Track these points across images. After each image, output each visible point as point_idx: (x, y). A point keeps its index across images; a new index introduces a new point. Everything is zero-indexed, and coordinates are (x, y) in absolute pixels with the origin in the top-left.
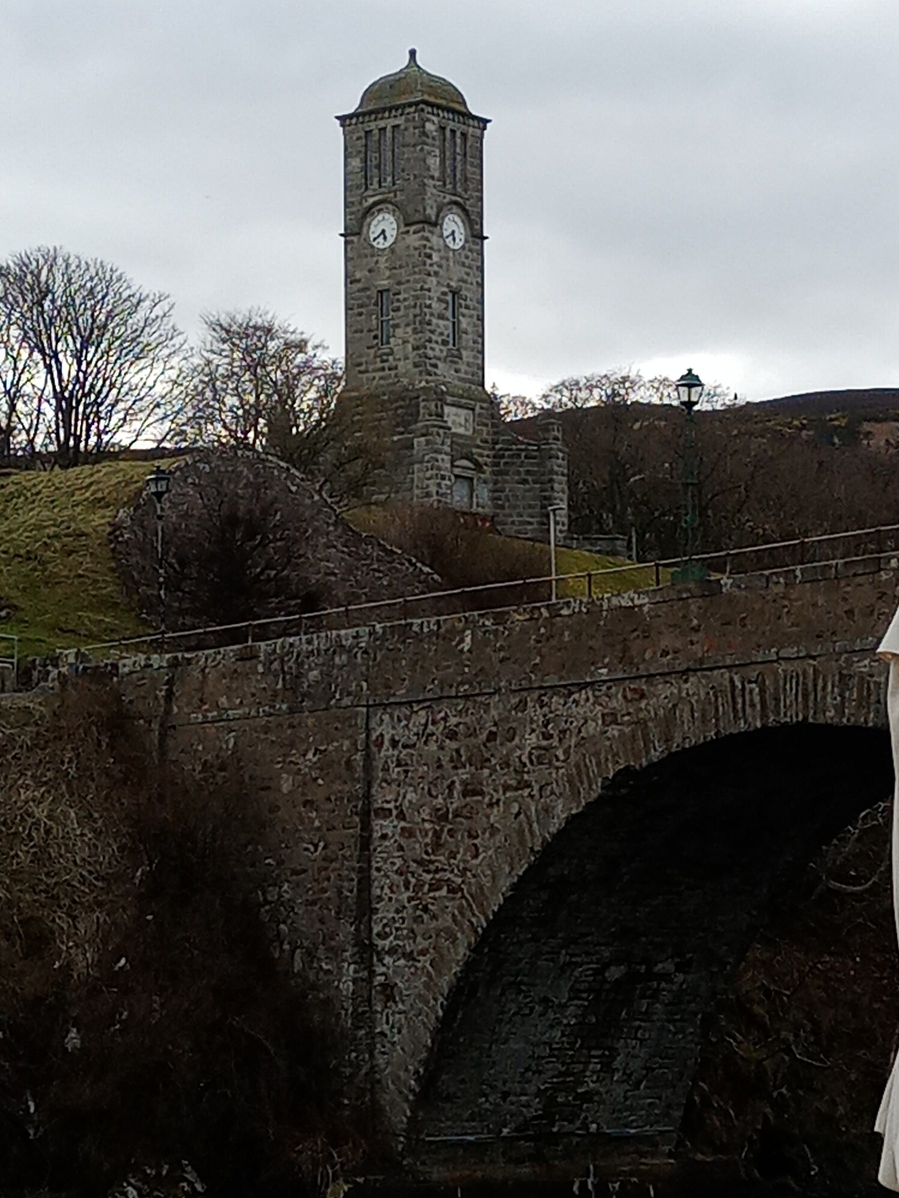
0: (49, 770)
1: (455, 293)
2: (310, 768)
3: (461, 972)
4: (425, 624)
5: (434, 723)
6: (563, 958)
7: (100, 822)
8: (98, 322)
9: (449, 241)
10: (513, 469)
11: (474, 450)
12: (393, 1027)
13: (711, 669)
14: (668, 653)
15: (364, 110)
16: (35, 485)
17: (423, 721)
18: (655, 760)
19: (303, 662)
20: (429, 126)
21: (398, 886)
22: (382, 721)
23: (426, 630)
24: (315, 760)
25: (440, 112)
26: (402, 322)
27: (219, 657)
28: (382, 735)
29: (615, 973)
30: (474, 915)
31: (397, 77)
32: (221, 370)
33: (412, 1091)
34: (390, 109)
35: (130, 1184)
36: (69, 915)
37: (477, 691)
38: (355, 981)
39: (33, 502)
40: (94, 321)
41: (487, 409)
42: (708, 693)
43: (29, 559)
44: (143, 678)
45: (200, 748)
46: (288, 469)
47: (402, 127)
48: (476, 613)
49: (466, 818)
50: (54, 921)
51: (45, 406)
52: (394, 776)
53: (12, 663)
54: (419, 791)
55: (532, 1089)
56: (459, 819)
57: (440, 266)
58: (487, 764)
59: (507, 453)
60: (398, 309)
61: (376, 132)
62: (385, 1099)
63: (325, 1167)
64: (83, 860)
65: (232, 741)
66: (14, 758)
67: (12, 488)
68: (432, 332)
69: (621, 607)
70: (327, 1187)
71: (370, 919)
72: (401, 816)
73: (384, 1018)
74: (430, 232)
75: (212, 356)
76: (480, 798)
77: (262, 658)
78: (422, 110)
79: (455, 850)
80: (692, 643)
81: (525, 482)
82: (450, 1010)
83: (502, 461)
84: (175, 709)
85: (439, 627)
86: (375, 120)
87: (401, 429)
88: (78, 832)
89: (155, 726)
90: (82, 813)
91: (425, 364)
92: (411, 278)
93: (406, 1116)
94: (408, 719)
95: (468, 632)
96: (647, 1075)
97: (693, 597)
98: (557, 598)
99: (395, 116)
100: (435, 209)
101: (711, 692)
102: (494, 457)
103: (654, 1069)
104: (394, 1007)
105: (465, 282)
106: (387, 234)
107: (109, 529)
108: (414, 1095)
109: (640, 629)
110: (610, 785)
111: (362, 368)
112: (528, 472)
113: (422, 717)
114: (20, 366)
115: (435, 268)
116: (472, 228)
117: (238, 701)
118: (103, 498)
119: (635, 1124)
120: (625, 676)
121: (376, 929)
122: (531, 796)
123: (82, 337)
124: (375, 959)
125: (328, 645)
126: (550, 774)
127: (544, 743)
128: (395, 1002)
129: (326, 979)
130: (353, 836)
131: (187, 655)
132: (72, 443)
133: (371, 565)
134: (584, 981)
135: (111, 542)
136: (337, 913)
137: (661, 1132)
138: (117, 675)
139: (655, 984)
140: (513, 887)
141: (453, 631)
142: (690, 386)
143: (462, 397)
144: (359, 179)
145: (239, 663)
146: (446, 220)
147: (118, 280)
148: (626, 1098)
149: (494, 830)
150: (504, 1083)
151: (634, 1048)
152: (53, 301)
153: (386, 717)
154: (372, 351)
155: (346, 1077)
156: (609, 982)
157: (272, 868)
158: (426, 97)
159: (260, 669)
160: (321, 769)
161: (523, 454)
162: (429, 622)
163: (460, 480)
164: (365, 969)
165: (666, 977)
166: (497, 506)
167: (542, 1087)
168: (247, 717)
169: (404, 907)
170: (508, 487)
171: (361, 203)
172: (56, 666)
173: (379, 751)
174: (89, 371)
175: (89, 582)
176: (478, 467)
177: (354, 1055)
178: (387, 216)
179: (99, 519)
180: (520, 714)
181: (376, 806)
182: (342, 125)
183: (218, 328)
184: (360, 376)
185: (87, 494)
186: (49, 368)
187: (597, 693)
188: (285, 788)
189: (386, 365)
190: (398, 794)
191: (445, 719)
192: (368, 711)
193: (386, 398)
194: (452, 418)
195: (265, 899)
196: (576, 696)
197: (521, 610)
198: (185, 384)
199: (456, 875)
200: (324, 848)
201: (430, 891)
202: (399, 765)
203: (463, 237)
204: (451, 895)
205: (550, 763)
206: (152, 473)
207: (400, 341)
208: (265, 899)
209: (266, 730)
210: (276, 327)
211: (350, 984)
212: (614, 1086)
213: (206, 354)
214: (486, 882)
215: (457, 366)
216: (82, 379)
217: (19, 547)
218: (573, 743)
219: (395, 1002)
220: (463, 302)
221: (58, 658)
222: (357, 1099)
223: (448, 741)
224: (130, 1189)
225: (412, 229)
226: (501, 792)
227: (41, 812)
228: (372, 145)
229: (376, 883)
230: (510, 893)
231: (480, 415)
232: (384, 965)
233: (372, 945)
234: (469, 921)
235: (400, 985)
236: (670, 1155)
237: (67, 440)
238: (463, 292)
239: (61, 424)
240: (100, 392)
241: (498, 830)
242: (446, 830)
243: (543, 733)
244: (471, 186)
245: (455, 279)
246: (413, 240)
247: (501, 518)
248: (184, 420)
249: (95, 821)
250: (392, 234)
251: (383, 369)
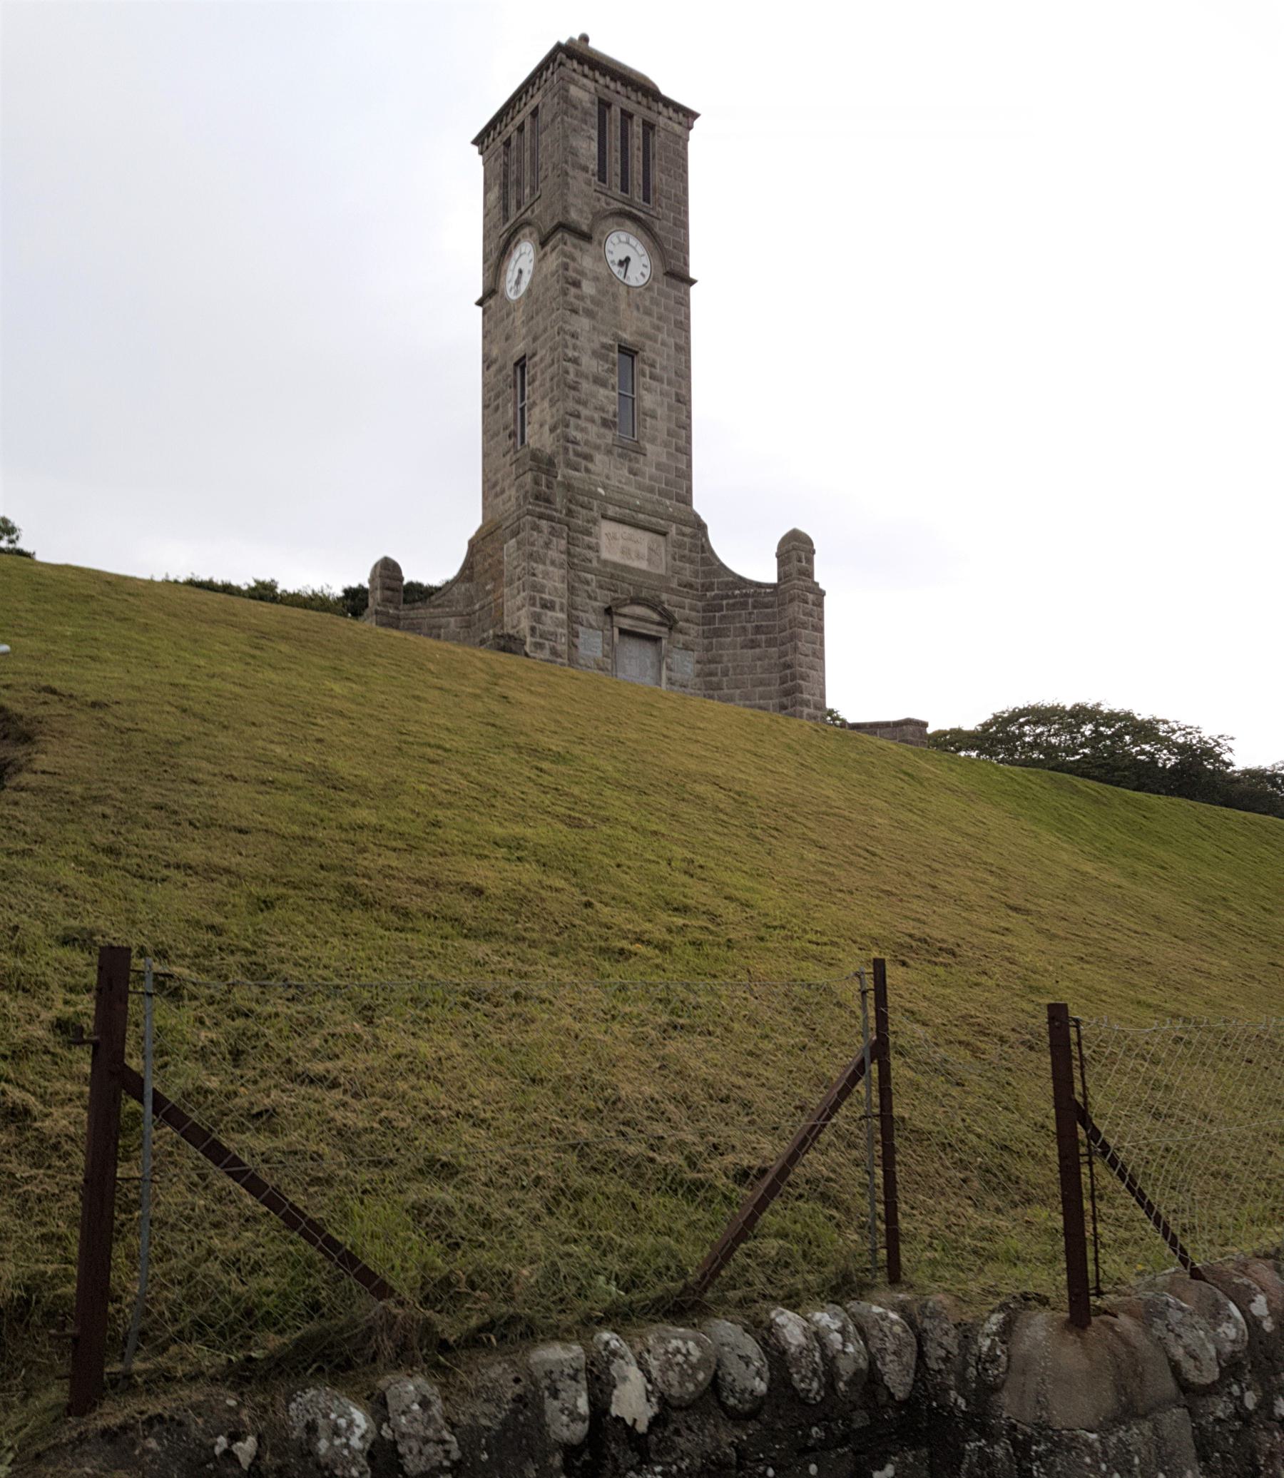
74: (575, 246)
81: (753, 644)
170: (726, 654)
238: (647, 354)
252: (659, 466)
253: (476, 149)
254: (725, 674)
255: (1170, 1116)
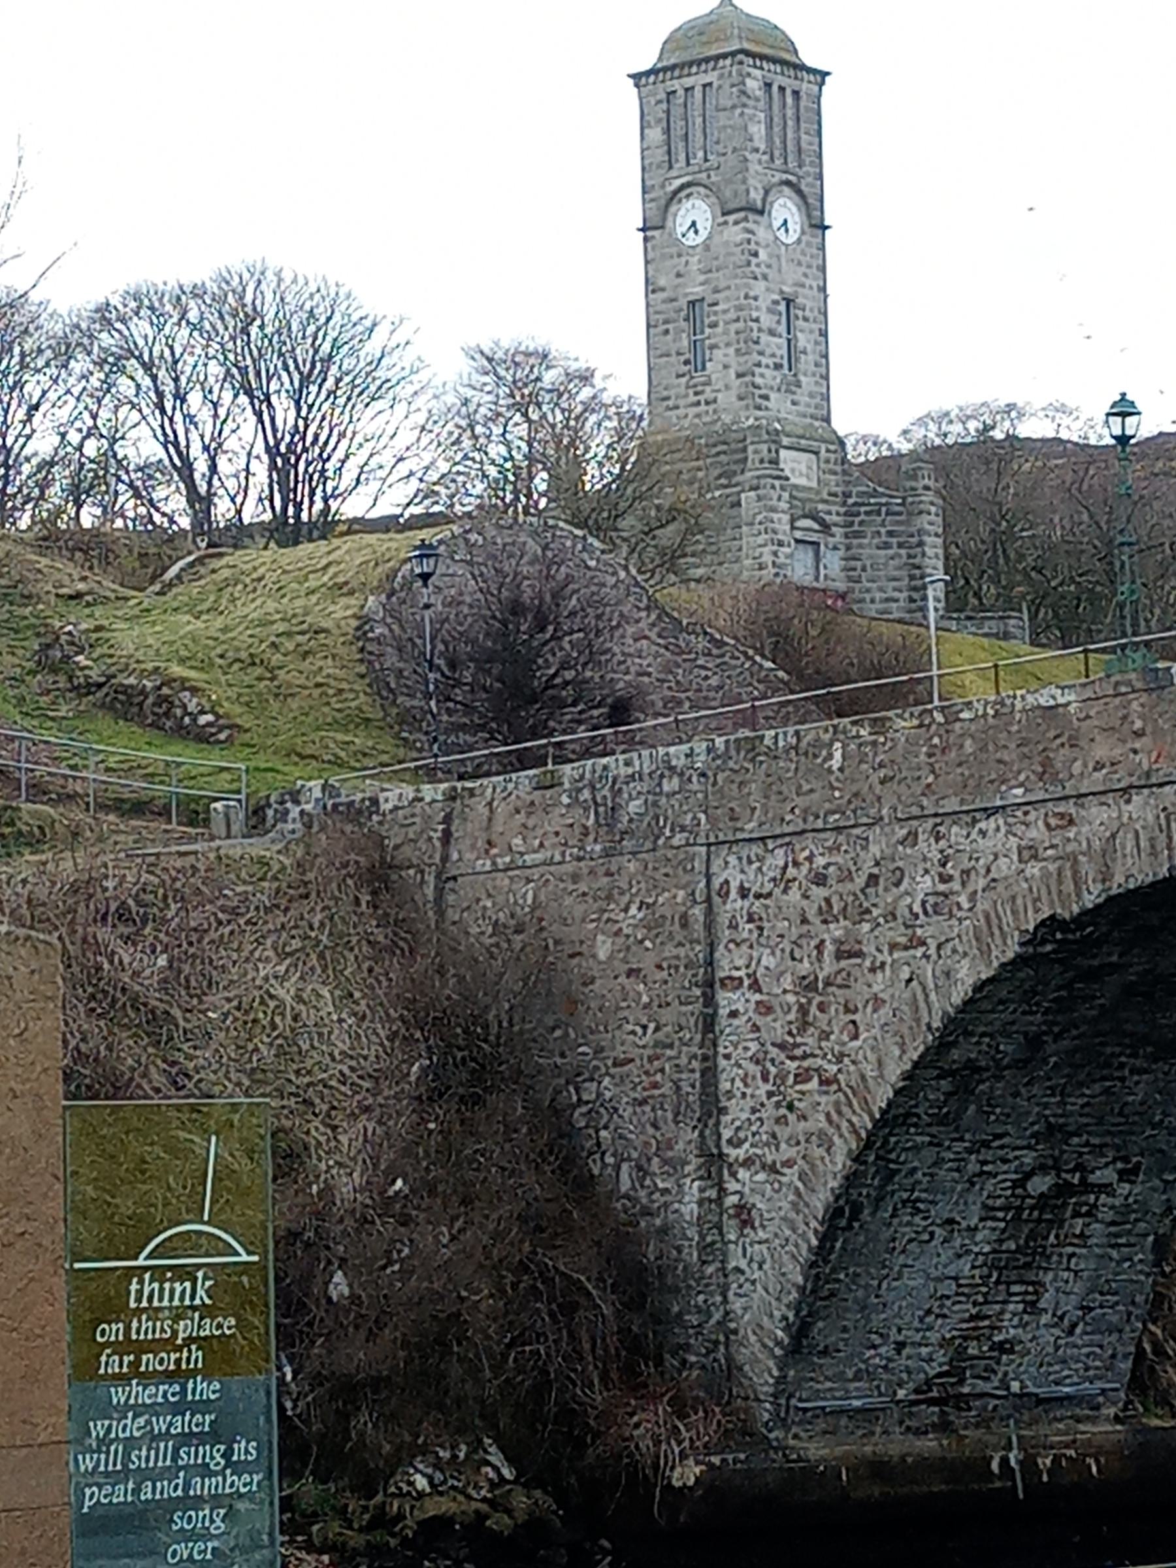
0: (293, 937)
1: (789, 302)
2: (636, 926)
3: (841, 1186)
4: (781, 737)
5: (796, 864)
6: (972, 1167)
7: (363, 1002)
8: (321, 354)
9: (781, 234)
10: (869, 530)
11: (820, 507)
12: (751, 1260)
13: (1161, 785)
14: (1103, 767)
15: (665, 63)
16: (255, 569)
17: (781, 863)
18: (1090, 906)
19: (620, 790)
20: (751, 84)
21: (754, 1078)
22: (727, 863)
23: (781, 744)
24: (640, 915)
25: (765, 65)
26: (720, 340)
27: (511, 786)
28: (727, 882)
29: (1040, 1184)
30: (854, 1112)
31: (707, 20)
32: (483, 410)
33: (778, 1343)
34: (699, 63)
35: (417, 1471)
36: (327, 1125)
37: (852, 822)
38: (700, 1203)
39: (255, 590)
40: (316, 352)
41: (835, 452)
42: (1158, 817)
43: (254, 664)
44: (413, 815)
45: (489, 904)
46: (584, 538)
47: (715, 85)
48: (847, 720)
49: (840, 987)
50: (308, 1133)
51: (255, 466)
52: (745, 935)
53: (239, 801)
54: (778, 953)
55: (934, 1336)
56: (831, 989)
57: (769, 266)
58: (867, 917)
59: (863, 509)
60: (713, 325)
61: (681, 92)
62: (743, 1355)
63: (669, 1444)
64: (342, 1053)
65: (531, 893)
66: (248, 923)
67: (226, 573)
68: (761, 353)
69: (1039, 707)
70: (673, 1468)
71: (718, 1123)
72: (756, 986)
73: (740, 1250)
74: (755, 222)
75: (469, 393)
76: (858, 961)
77: (567, 786)
78: (741, 63)
79: (827, 1029)
80: (1135, 752)
81: (887, 546)
82: (826, 1238)
83: (857, 520)
84: (455, 856)
85: (799, 740)
86: (680, 77)
87: (723, 481)
88: (335, 1017)
89: (431, 879)
90: (337, 993)
91: (752, 396)
92: (732, 283)
93: (772, 1376)
94: (760, 859)
95: (838, 745)
96: (1083, 1318)
97: (1134, 691)
98: (941, 699)
99: (705, 71)
100: (762, 192)
101: (1162, 816)
102: (845, 514)
103: (1091, 1309)
104: (752, 1234)
105: (803, 286)
106: (699, 226)
107: (355, 623)
108: (782, 1348)
109: (1067, 735)
110: (1033, 940)
111: (671, 403)
112: (890, 534)
113: (779, 858)
114: (222, 412)
115: (764, 269)
116: (809, 216)
117: (537, 842)
118: (346, 583)
119: (1068, 1381)
120: (1047, 796)
121: (727, 1134)
122: (926, 957)
123: (301, 373)
124: (726, 1172)
125: (654, 767)
126: (950, 927)
127: (942, 887)
128: (753, 1228)
129: (663, 1199)
130: (692, 1014)
131: (469, 785)
132: (291, 511)
133: (695, 660)
134: (1000, 1196)
135: (358, 639)
136: (677, 1114)
137: (1103, 1391)
138: (377, 813)
139: (1092, 1197)
140: (908, 1076)
141: (817, 743)
142: (1124, 415)
143: (802, 437)
144: (660, 155)
145: (538, 793)
146: (776, 206)
147: (348, 296)
148: (1057, 1348)
149: (878, 1002)
150: (900, 1330)
151: (1067, 1282)
152: (262, 327)
153: (732, 860)
154: (684, 380)
155: (693, 1327)
156: (1032, 1197)
157: (588, 1058)
158: (747, 46)
159: (565, 800)
160: (649, 929)
161: (884, 509)
162: (785, 734)
163: (801, 546)
164: (712, 1187)
165: (1106, 1188)
166: (850, 579)
167: (948, 1336)
168: (550, 862)
169: (762, 1105)
171: (663, 186)
172: (297, 802)
173: (724, 903)
174: (311, 416)
175: (331, 692)
176: (826, 528)
177: (701, 1298)
178: (698, 203)
179: (342, 611)
180: (909, 851)
181: (722, 974)
182: (637, 85)
183: (478, 356)
184: (670, 413)
185: (325, 579)
186: (259, 415)
187: (1011, 820)
188: (602, 955)
189: (701, 398)
190: (751, 958)
191: (810, 859)
192: (708, 854)
193: (703, 441)
194: (791, 465)
195: (579, 1100)
196: (983, 825)
197: (907, 715)
198: (437, 429)
199: (830, 1061)
200: (657, 1029)
201: (796, 1083)
202: (750, 920)
203: (798, 228)
204: (824, 1088)
205: (951, 915)
206: (416, 548)
207: (720, 367)
208: (579, 1100)
209: (575, 878)
210: (554, 353)
211: (695, 1206)
212: (1043, 1331)
213: (462, 390)
214: (870, 1071)
215: (795, 397)
216: (301, 429)
217: (238, 650)
218: (980, 888)
219: (753, 1228)
220: (800, 313)
221: (299, 792)
222: (706, 1355)
223: (814, 887)
224: (418, 1477)
225: (731, 218)
226: (886, 953)
227: (285, 992)
228: (677, 111)
229: (724, 1076)
230: (901, 1084)
231: (827, 461)
232: (738, 1181)
233: (721, 1155)
234: (849, 1121)
235: (759, 1206)
236: (1117, 1419)
237: (285, 509)
238: (799, 301)
239: (276, 487)
240: (326, 443)
241: (884, 1002)
242: (815, 1003)
243: (940, 875)
244: (808, 160)
245: (790, 282)
246: (734, 233)
247: (857, 595)
248: (435, 478)
249: (356, 1003)
250: (704, 227)
251: (698, 403)
252: (811, 395)
253: (630, 94)
254: (864, 569)
255: (726, 1276)
